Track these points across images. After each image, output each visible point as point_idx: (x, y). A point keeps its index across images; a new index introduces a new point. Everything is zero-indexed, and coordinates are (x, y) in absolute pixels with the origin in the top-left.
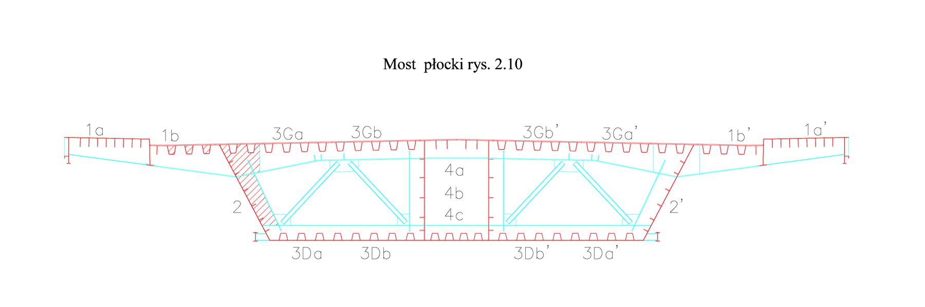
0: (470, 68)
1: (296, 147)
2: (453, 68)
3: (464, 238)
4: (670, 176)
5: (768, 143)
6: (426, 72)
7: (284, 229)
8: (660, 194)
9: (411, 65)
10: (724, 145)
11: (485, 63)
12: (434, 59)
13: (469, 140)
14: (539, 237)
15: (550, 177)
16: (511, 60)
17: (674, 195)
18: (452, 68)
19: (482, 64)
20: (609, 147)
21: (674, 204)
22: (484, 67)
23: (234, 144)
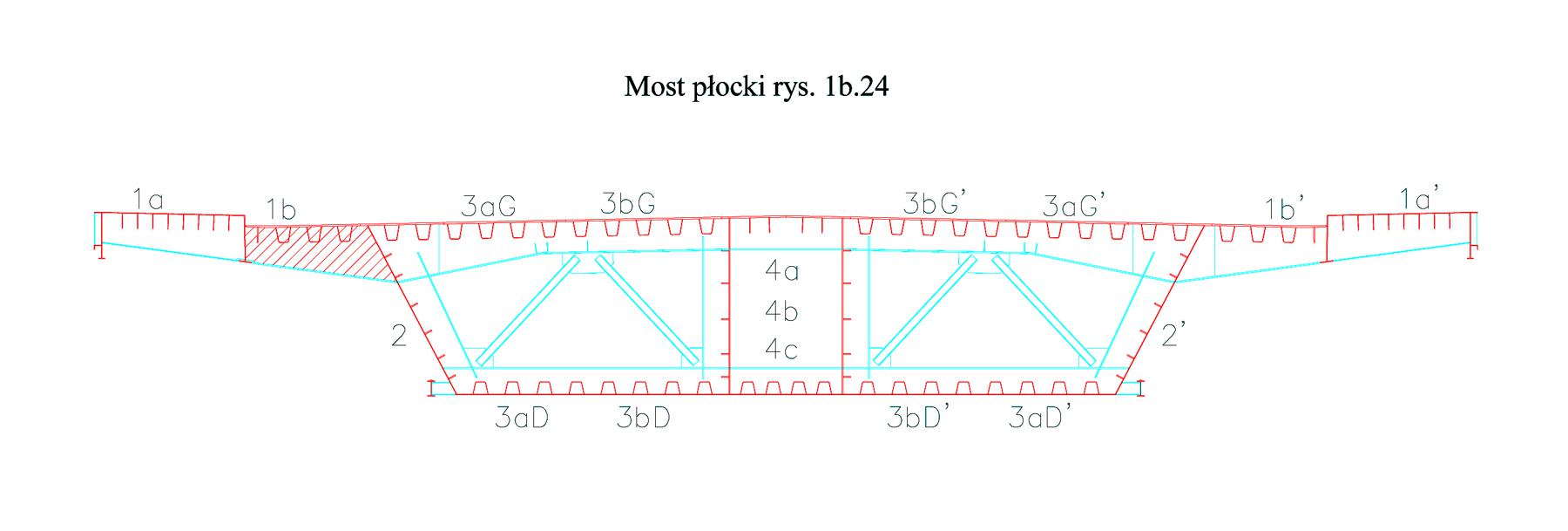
0: (777, 94)
1: (502, 230)
2: (746, 94)
3: (799, 391)
4: (1164, 280)
5: (1335, 223)
6: (696, 100)
7: (482, 375)
8: (1141, 315)
9: (677, 88)
10: (391, 224)
11: (806, 83)
12: (711, 77)
13: (734, 217)
14: (640, 389)
15: (947, 286)
16: (831, 78)
17: (1171, 314)
18: (744, 93)
19: (800, 87)
20: (1054, 228)
21: (400, 330)
22: (803, 92)
23: (1150, 224)
